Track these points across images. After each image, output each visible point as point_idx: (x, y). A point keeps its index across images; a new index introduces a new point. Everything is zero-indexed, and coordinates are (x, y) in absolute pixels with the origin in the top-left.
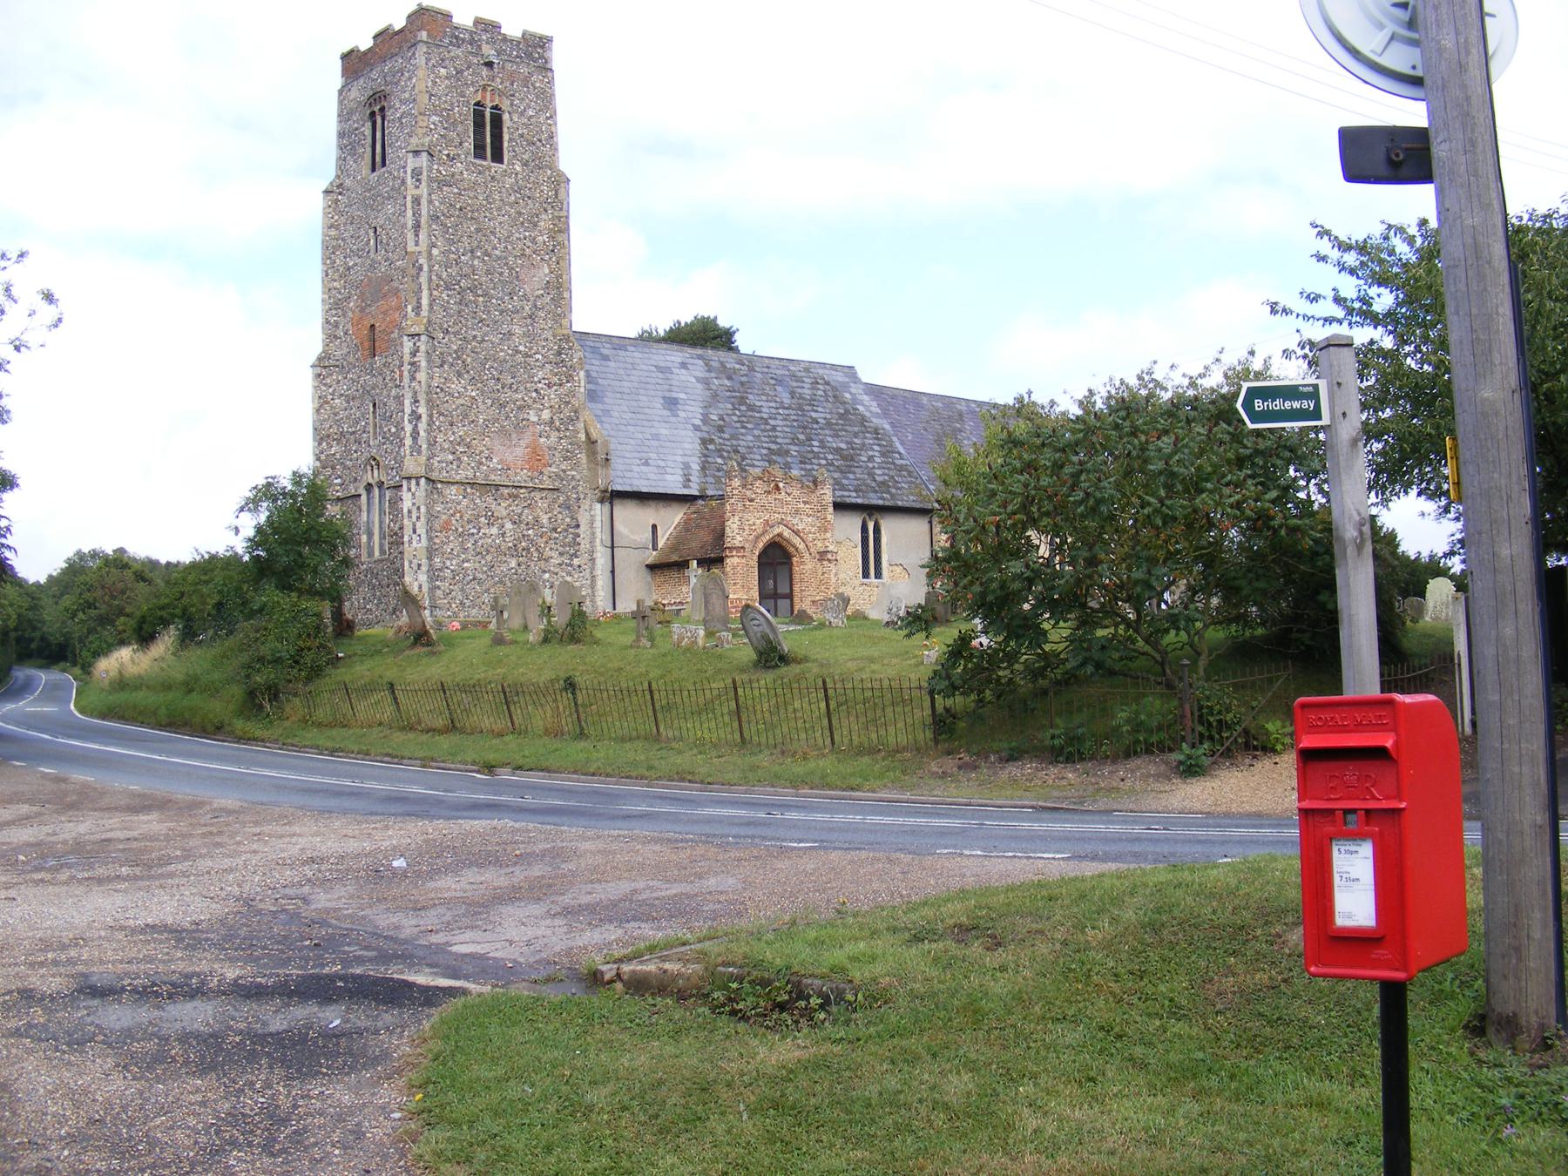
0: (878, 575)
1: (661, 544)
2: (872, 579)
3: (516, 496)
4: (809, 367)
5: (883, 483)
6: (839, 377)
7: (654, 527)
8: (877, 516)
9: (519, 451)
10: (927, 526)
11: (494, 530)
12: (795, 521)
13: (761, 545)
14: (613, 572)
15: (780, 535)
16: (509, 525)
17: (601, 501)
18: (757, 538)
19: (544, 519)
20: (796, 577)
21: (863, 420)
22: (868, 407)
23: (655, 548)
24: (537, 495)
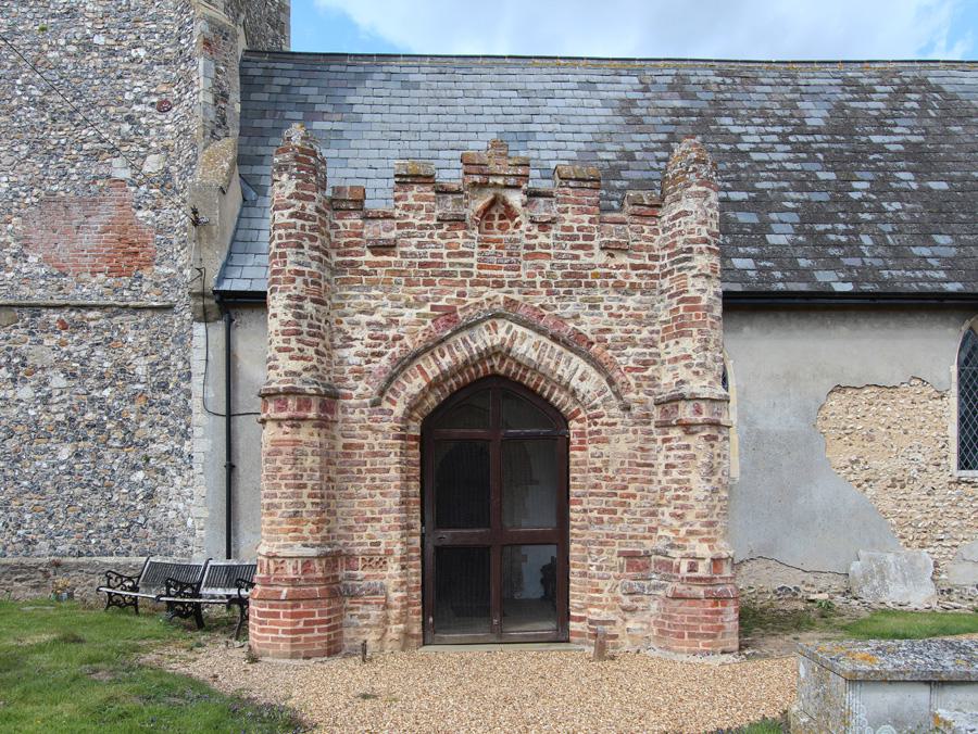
3: (79, 326)
9: (88, 239)
11: (26, 392)
14: (231, 468)
16: (58, 381)
17: (204, 317)
19: (141, 367)
24: (127, 321)
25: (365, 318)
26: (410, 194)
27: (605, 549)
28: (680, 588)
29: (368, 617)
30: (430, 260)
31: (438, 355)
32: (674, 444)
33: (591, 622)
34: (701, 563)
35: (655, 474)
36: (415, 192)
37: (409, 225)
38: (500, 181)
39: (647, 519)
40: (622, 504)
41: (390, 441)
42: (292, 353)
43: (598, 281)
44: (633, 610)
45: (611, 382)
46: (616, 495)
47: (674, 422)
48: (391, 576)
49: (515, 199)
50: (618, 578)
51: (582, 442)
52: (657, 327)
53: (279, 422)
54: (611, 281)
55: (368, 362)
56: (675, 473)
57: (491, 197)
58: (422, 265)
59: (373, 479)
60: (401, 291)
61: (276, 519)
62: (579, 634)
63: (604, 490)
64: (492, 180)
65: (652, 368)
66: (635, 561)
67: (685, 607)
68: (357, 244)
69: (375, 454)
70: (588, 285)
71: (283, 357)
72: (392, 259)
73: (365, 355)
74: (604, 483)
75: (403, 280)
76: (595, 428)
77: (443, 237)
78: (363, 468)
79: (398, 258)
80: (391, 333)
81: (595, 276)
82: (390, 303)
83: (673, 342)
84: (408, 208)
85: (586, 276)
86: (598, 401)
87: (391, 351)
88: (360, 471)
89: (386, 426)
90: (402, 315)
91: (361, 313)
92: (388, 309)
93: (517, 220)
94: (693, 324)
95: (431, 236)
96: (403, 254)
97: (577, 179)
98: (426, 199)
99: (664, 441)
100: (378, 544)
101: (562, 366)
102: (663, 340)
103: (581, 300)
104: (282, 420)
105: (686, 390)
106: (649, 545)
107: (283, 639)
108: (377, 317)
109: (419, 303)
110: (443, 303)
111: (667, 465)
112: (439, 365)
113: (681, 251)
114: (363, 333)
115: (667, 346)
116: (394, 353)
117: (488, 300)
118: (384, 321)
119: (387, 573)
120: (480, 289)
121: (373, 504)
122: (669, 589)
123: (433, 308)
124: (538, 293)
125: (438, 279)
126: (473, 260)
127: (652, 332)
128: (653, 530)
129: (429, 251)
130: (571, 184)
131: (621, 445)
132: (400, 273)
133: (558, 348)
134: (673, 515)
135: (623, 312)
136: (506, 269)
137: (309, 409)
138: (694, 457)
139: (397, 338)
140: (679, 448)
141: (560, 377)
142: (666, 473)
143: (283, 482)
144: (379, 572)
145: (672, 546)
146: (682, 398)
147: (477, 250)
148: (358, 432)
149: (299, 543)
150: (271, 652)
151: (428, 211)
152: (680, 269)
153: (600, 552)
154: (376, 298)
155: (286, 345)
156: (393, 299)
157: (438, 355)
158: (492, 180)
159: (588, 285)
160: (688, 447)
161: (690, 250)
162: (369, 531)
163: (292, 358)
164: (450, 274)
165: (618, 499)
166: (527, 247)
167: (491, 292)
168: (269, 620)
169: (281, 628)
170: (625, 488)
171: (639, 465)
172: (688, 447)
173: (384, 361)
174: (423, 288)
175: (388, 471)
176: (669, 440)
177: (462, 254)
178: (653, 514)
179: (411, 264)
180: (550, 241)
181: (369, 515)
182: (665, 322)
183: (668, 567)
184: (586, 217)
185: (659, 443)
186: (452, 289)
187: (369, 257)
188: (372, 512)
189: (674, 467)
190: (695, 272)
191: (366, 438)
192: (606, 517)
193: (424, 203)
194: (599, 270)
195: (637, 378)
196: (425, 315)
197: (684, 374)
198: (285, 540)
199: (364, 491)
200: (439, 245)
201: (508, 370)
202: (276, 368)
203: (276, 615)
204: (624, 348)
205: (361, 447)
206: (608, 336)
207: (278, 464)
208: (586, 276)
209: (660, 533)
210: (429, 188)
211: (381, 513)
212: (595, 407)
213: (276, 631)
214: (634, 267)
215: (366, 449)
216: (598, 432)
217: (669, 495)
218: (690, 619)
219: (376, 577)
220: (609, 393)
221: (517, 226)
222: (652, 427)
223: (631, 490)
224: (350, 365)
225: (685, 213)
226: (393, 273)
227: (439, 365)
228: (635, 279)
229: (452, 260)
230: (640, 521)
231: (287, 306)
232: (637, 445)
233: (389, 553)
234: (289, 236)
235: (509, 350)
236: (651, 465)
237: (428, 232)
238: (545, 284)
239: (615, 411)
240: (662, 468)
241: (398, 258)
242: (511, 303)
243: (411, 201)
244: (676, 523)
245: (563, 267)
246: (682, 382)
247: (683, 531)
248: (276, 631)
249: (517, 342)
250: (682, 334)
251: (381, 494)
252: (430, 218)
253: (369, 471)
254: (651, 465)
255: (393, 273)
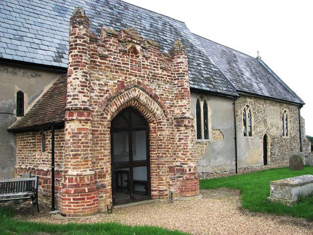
0: (206, 137)
1: (27, 110)
2: (203, 140)
4: (161, 17)
5: (207, 78)
6: (178, 25)
7: (20, 96)
8: (205, 98)
10: (232, 106)
12: (153, 86)
13: (113, 109)
14: (235, 138)
15: (136, 99)
18: (109, 100)
20: (154, 144)
21: (192, 46)
22: (193, 40)
23: (20, 112)
25: (97, 82)
26: (111, 40)
27: (164, 166)
28: (188, 176)
29: (102, 197)
30: (117, 64)
31: (120, 98)
32: (182, 132)
33: (160, 191)
34: (192, 169)
35: (175, 141)
36: (112, 40)
37: (111, 51)
38: (135, 41)
39: (173, 156)
40: (168, 151)
41: (106, 129)
42: (84, 94)
43: (160, 79)
44: (172, 185)
45: (164, 111)
46: (166, 148)
47: (183, 125)
48: (107, 181)
49: (138, 48)
50: (167, 175)
51: (155, 131)
52: (173, 95)
53: (80, 121)
54: (163, 79)
55: (99, 99)
56: (183, 141)
57: (131, 46)
58: (115, 66)
59: (101, 144)
60: (108, 73)
61: (79, 160)
62: (156, 195)
63: (163, 147)
64: (133, 41)
65: (173, 108)
66: (171, 169)
67: (189, 182)
68: (96, 55)
69: (102, 134)
70: (158, 79)
71: (81, 95)
72: (106, 62)
73: (98, 96)
74: (163, 144)
75: (109, 70)
76: (161, 126)
77: (121, 57)
78: (98, 139)
79: (108, 62)
80: (105, 88)
81: (159, 77)
82: (105, 77)
83: (179, 101)
84: (111, 45)
85: (157, 77)
86: (161, 117)
87: (106, 95)
88: (97, 140)
89: (105, 123)
90: (109, 82)
91: (96, 80)
92: (105, 80)
93: (138, 55)
94: (186, 96)
95: (117, 56)
96: (110, 61)
97: (155, 46)
98: (116, 43)
99: (178, 131)
100: (103, 168)
101: (152, 105)
102: (175, 99)
103: (156, 84)
104: (82, 120)
105: (186, 115)
106: (175, 164)
107: (87, 208)
108: (101, 82)
109: (114, 78)
110: (120, 80)
111: (179, 139)
112: (120, 102)
113: (181, 73)
114: (97, 88)
115: (177, 102)
116: (107, 96)
117: (133, 80)
118: (103, 84)
119: (106, 180)
120: (131, 76)
121: (102, 153)
122: (184, 177)
123: (118, 81)
124: (146, 80)
125: (119, 71)
126: (129, 66)
127: (172, 96)
128: (175, 159)
129: (117, 61)
130: (153, 47)
131: (166, 132)
132: (108, 67)
133: (151, 99)
134: (182, 154)
135: (166, 89)
136: (138, 71)
137: (73, 116)
138: (188, 136)
139: (107, 91)
140: (184, 133)
141: (152, 109)
142: (179, 141)
143: (82, 145)
144: (103, 179)
145: (183, 164)
146: (185, 118)
147: (130, 63)
148: (96, 125)
149: (88, 169)
150: (81, 214)
151: (116, 47)
152: (181, 79)
153: (163, 167)
154: (102, 75)
155: (82, 91)
156: (106, 76)
157: (120, 98)
158: (133, 41)
159: (158, 79)
160: (187, 133)
161: (184, 74)
162: (100, 164)
163: (84, 96)
164: (123, 70)
165: (166, 149)
166: (143, 65)
167: (133, 78)
168: (80, 201)
169: (86, 204)
170: (168, 146)
171: (171, 138)
172: (187, 133)
173: (103, 98)
174: (115, 74)
175: (106, 140)
176: (180, 131)
177: (126, 64)
178: (175, 154)
179: (112, 65)
180: (148, 64)
181: (100, 157)
182: (176, 94)
183: (183, 171)
184: (156, 58)
185: (176, 131)
186: (123, 75)
187: (99, 60)
188: (101, 156)
189: (183, 139)
190: (185, 80)
191: (99, 127)
192: (164, 155)
193: (115, 44)
194: (160, 75)
195: (170, 111)
196: (116, 84)
197: (184, 111)
198: (83, 168)
199: (99, 148)
200: (120, 59)
201: (136, 105)
202: (78, 99)
203: (84, 199)
204: (166, 100)
205: (97, 131)
206: (163, 97)
207: (80, 138)
208: (157, 77)
209: (177, 160)
210: (117, 39)
211: (104, 156)
212: (160, 119)
213: (84, 205)
214: (168, 76)
215: (99, 132)
216: (162, 128)
217: (181, 148)
218: (191, 186)
219: (102, 181)
220: (163, 115)
221: (138, 57)
222: (173, 126)
223: (169, 147)
224: (93, 99)
225: (182, 63)
226: (107, 67)
227: (120, 102)
228: (168, 80)
229: (123, 65)
230: (172, 157)
231: (83, 76)
232: (170, 132)
233: (107, 171)
234: (83, 49)
235: (139, 98)
236: (174, 139)
237: (116, 54)
238: (148, 78)
239: (165, 121)
240: (178, 139)
241: (108, 62)
242: (139, 83)
243: (111, 43)
244: (184, 157)
245: (152, 73)
246: (184, 113)
247: (186, 159)
248: (84, 205)
249: (141, 96)
250: (183, 99)
251: (104, 149)
252: (117, 49)
253: (100, 140)
254: (174, 139)
255: (107, 67)
